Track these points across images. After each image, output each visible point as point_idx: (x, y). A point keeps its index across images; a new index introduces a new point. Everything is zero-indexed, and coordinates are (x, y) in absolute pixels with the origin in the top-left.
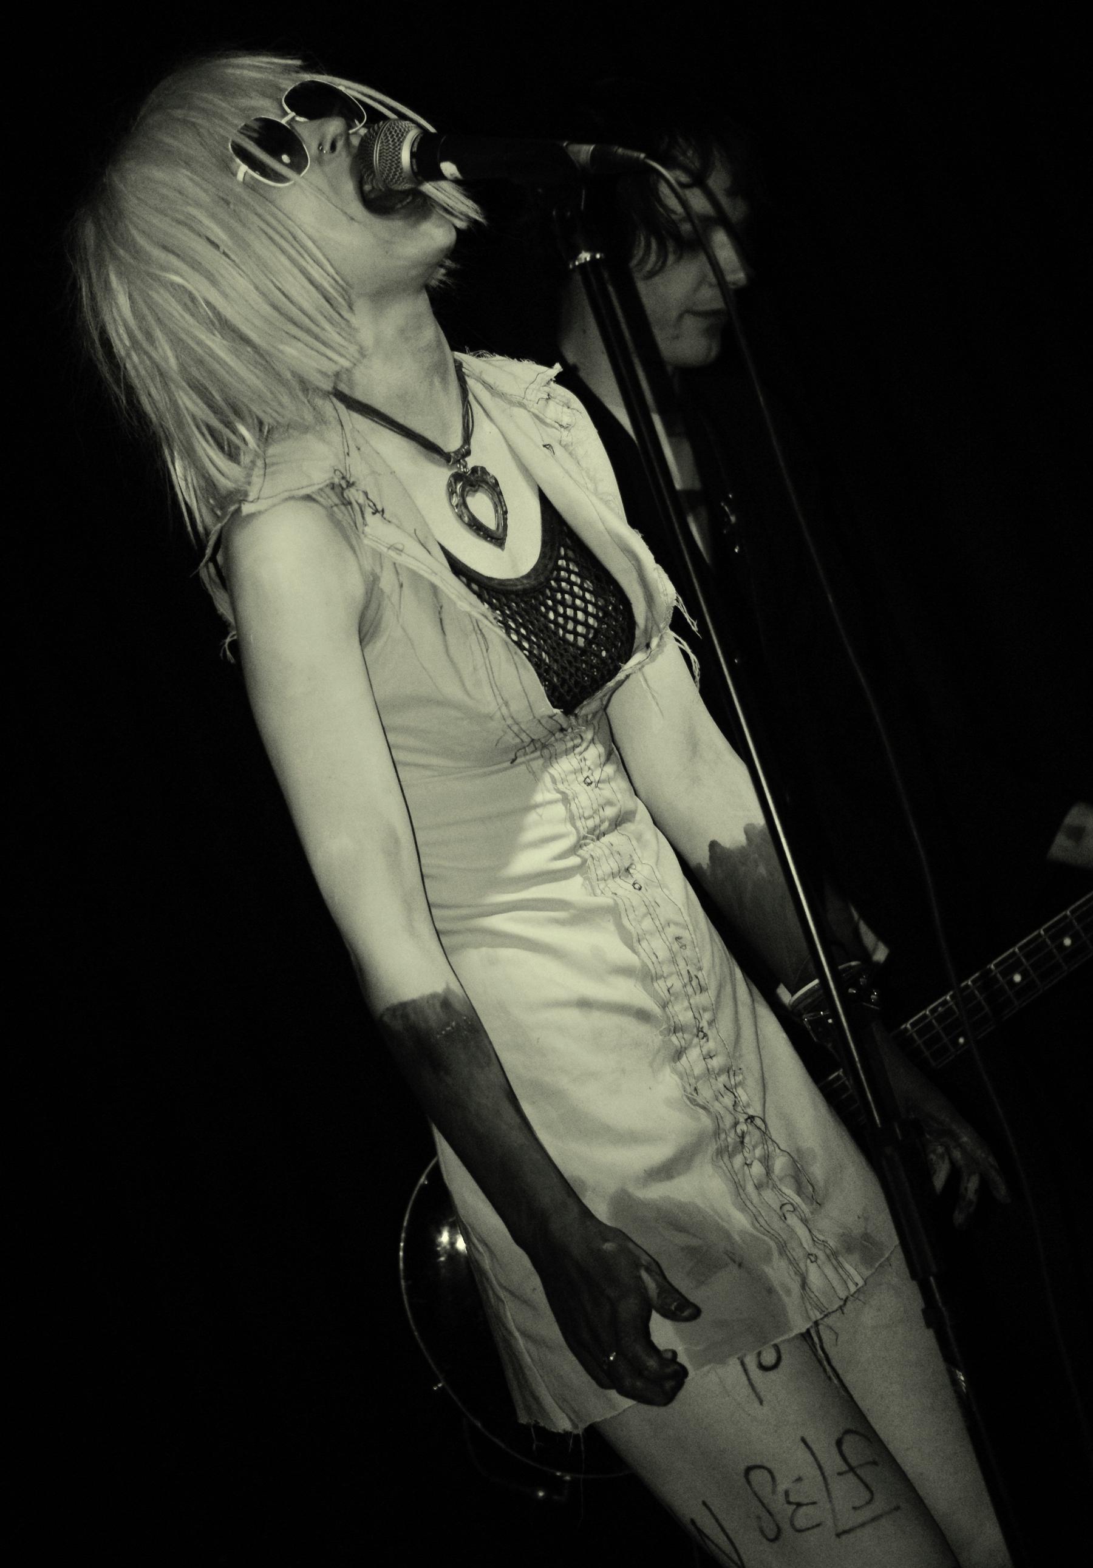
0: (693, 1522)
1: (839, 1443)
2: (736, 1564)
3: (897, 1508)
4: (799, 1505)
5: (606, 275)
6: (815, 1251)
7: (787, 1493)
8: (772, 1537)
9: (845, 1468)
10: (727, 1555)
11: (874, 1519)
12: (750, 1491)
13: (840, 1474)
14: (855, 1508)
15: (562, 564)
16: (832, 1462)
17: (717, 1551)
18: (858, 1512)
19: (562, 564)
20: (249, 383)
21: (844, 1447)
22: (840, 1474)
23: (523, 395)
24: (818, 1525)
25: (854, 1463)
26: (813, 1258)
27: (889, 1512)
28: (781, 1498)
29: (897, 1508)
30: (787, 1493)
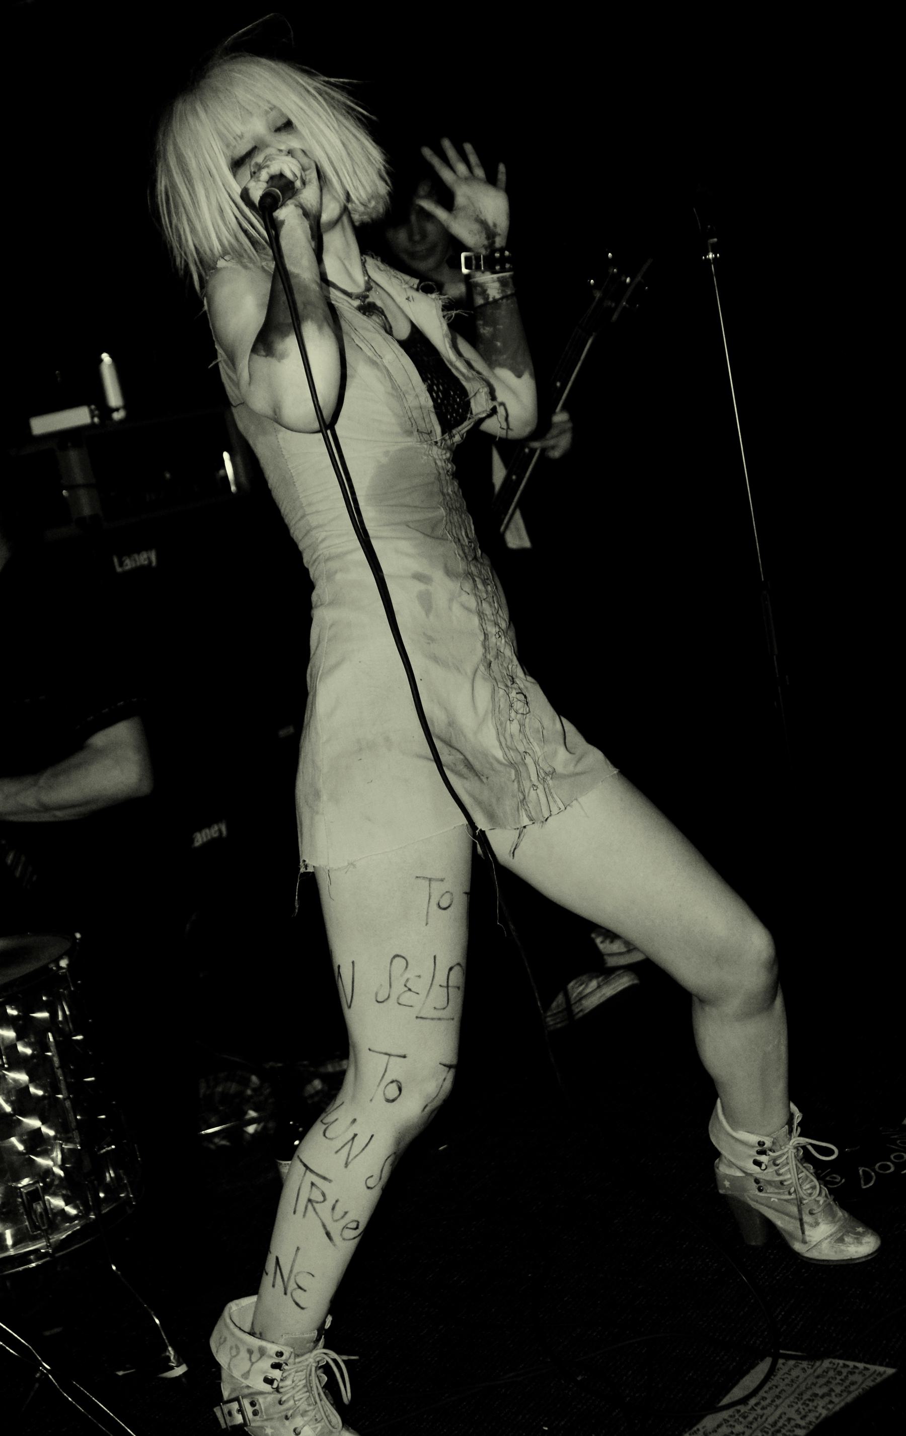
0: (339, 967)
1: (451, 969)
2: (347, 1004)
3: (453, 1019)
4: (410, 990)
5: (45, 1371)
6: (536, 783)
7: (407, 980)
8: (379, 1000)
9: (445, 984)
10: (346, 999)
11: (439, 1019)
12: (388, 969)
13: (440, 986)
14: (435, 1008)
15: (127, 565)
16: (441, 978)
17: (342, 989)
18: (435, 1011)
19: (127, 565)
20: (337, 136)
21: (451, 973)
22: (440, 986)
23: (504, 425)
24: (411, 1006)
25: (450, 984)
26: (535, 789)
27: (448, 1019)
28: (403, 981)
29: (453, 1019)
30: (407, 980)
